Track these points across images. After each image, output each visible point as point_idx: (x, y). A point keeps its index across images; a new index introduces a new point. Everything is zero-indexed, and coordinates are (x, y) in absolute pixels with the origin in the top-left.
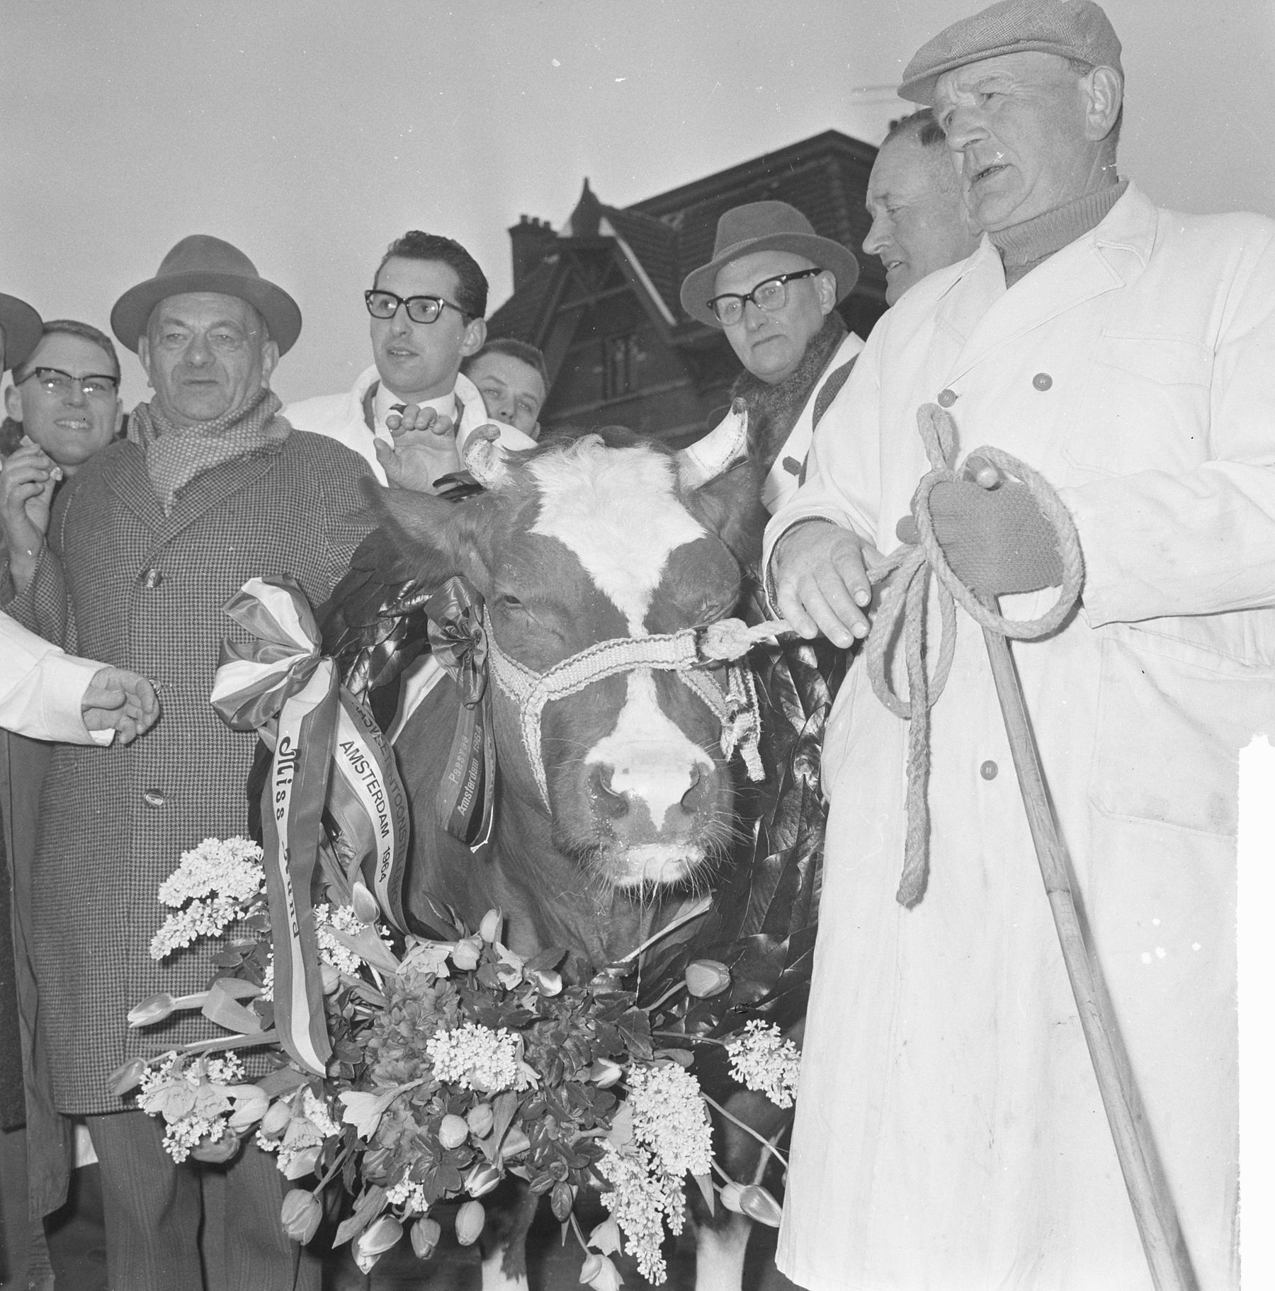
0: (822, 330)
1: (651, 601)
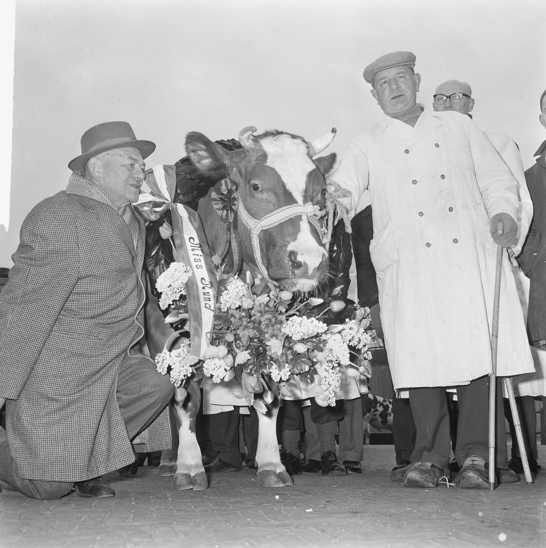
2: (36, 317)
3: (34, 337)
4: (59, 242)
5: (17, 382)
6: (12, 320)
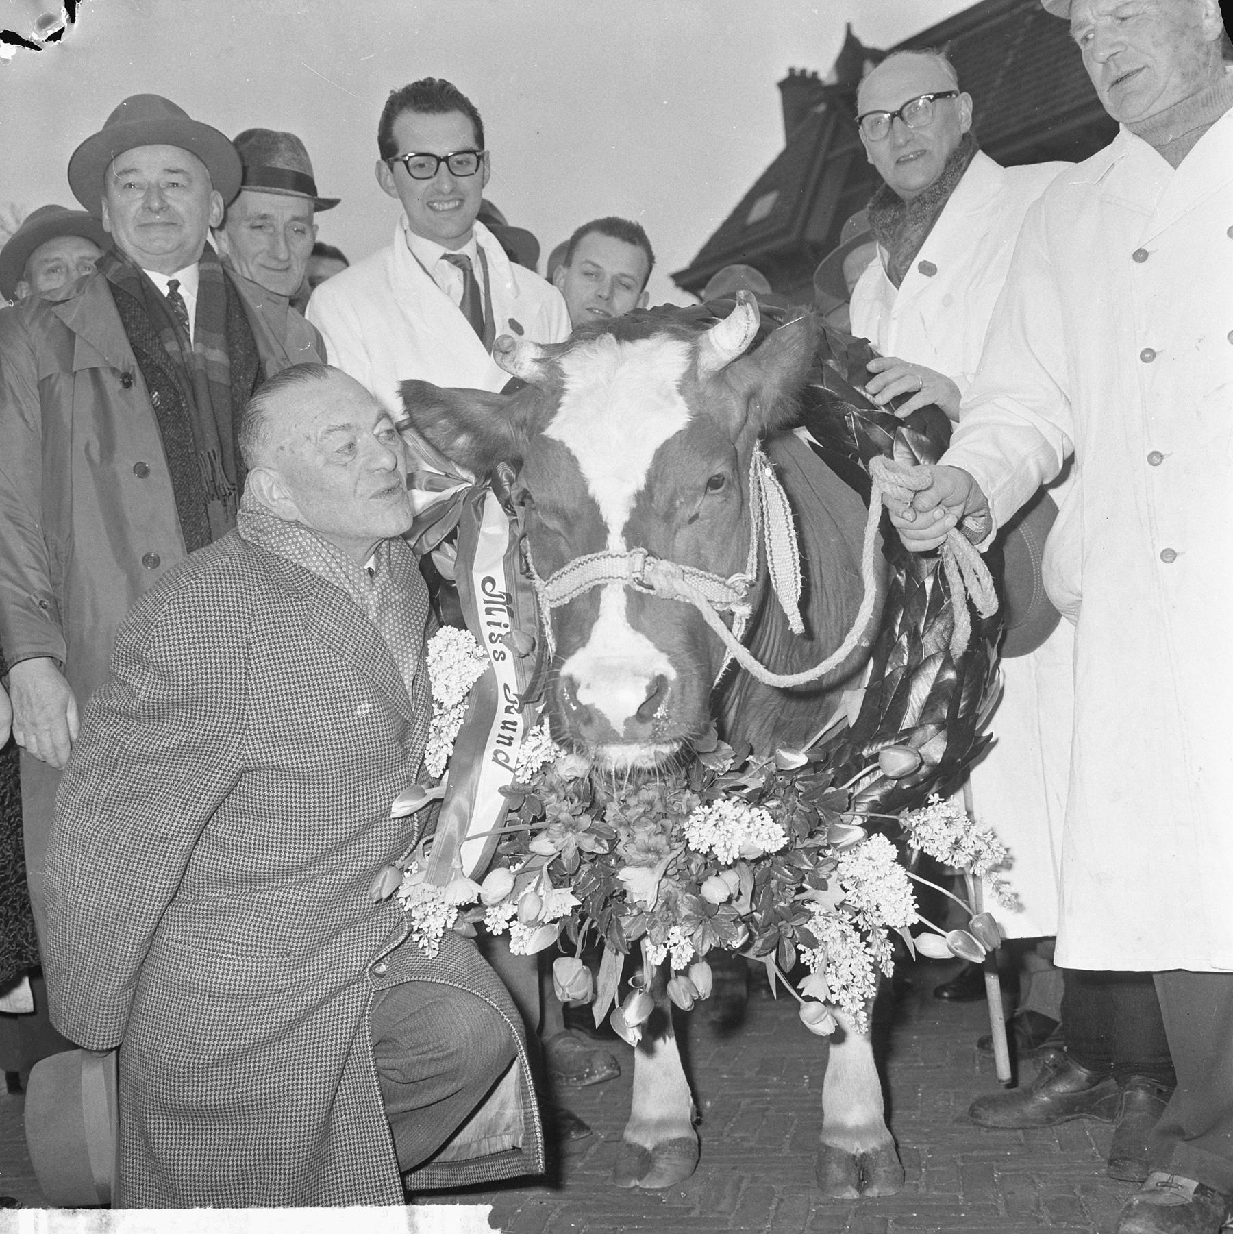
0: (960, 145)
1: (634, 505)
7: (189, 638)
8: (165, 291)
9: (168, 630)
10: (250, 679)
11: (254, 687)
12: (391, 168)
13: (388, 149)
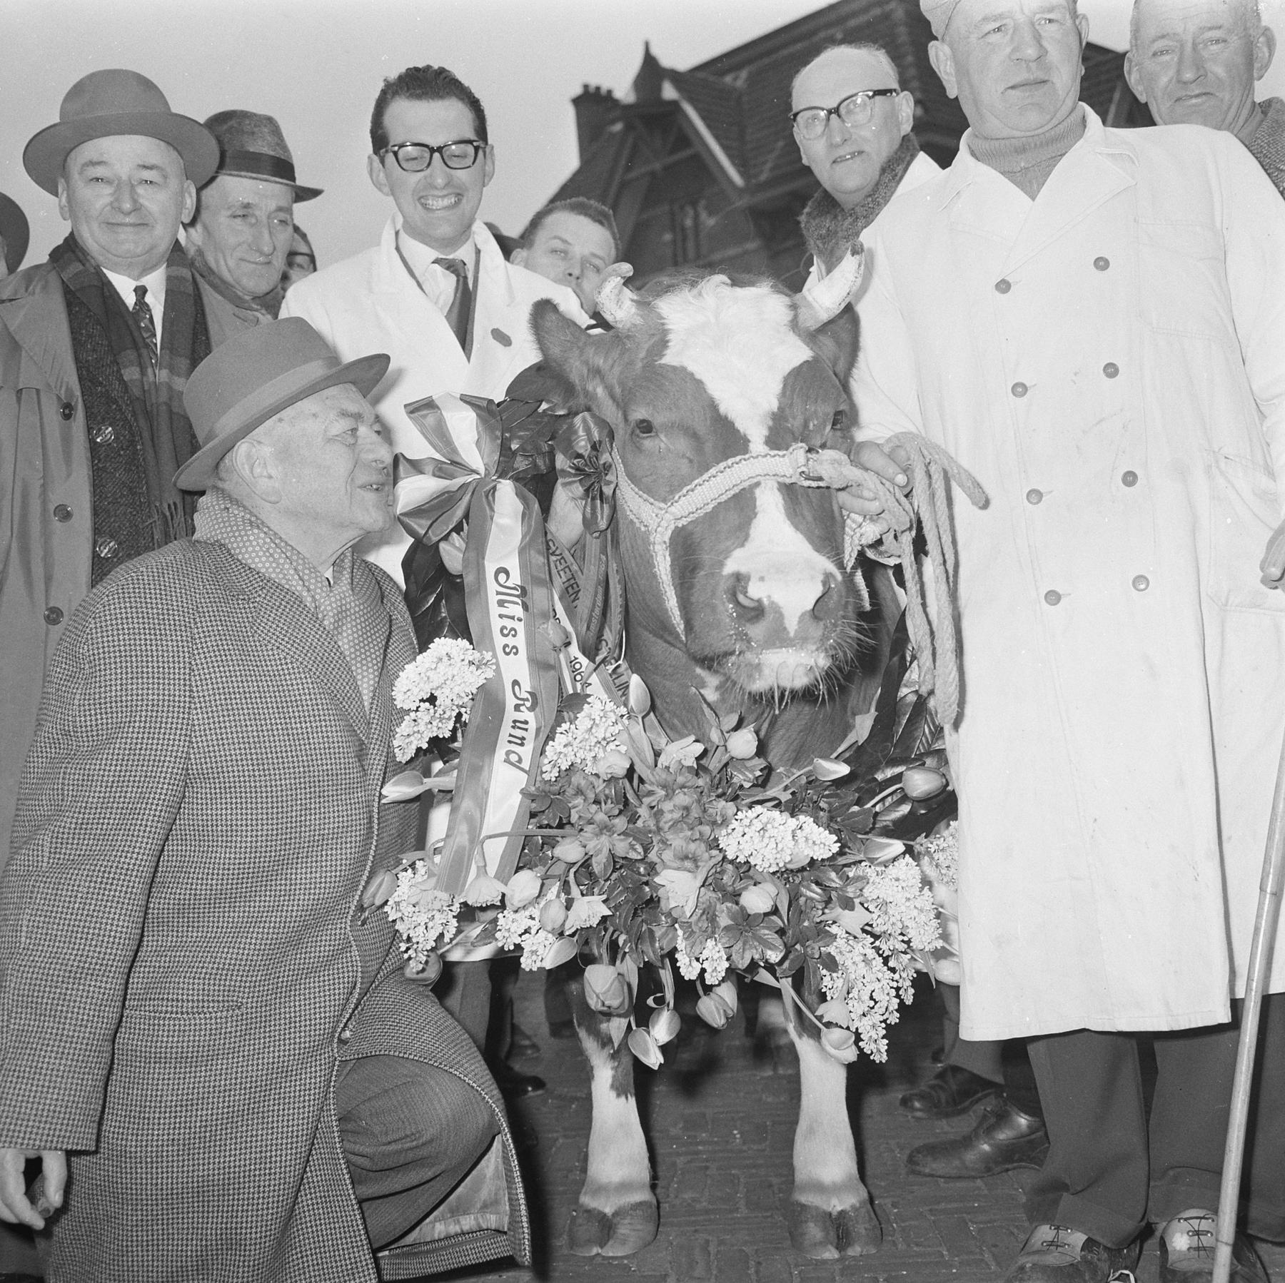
1: (771, 423)
2: (96, 905)
3: (96, 964)
4: (137, 678)
5: (66, 1098)
6: (31, 924)
7: (129, 629)
8: (130, 300)
9: (106, 621)
10: (195, 676)
11: (199, 683)
12: (382, 162)
13: (380, 140)
